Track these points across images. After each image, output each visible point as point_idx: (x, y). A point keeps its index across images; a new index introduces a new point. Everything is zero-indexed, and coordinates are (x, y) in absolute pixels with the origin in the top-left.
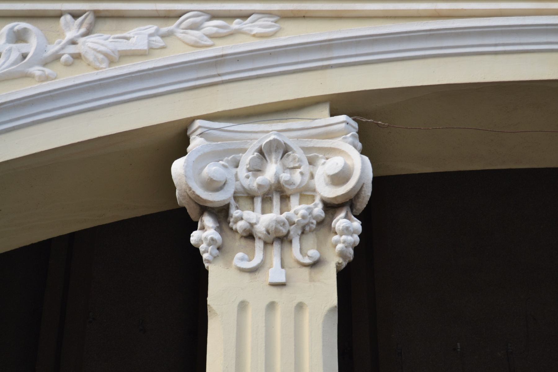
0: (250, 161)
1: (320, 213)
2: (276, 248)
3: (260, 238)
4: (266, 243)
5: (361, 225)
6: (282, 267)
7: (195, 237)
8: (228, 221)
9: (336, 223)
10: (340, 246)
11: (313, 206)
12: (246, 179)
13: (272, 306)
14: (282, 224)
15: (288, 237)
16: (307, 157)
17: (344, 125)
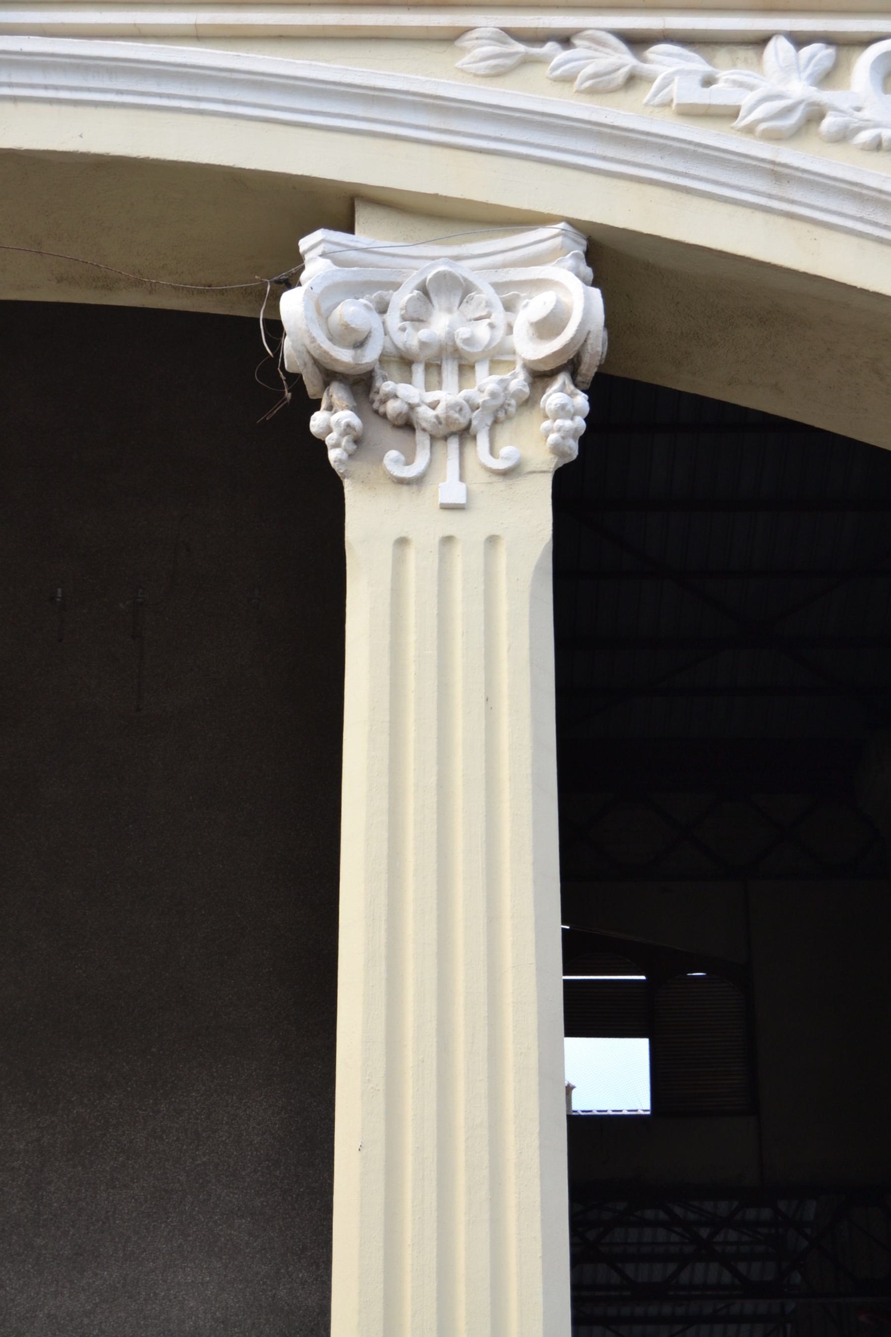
0: (407, 303)
1: (520, 387)
2: (453, 445)
3: (424, 430)
4: (433, 438)
5: (589, 401)
6: (462, 478)
7: (317, 422)
8: (370, 399)
9: (546, 400)
10: (553, 437)
11: (509, 377)
12: (400, 333)
13: (448, 540)
14: (458, 408)
15: (471, 430)
16: (500, 298)
17: (559, 240)
